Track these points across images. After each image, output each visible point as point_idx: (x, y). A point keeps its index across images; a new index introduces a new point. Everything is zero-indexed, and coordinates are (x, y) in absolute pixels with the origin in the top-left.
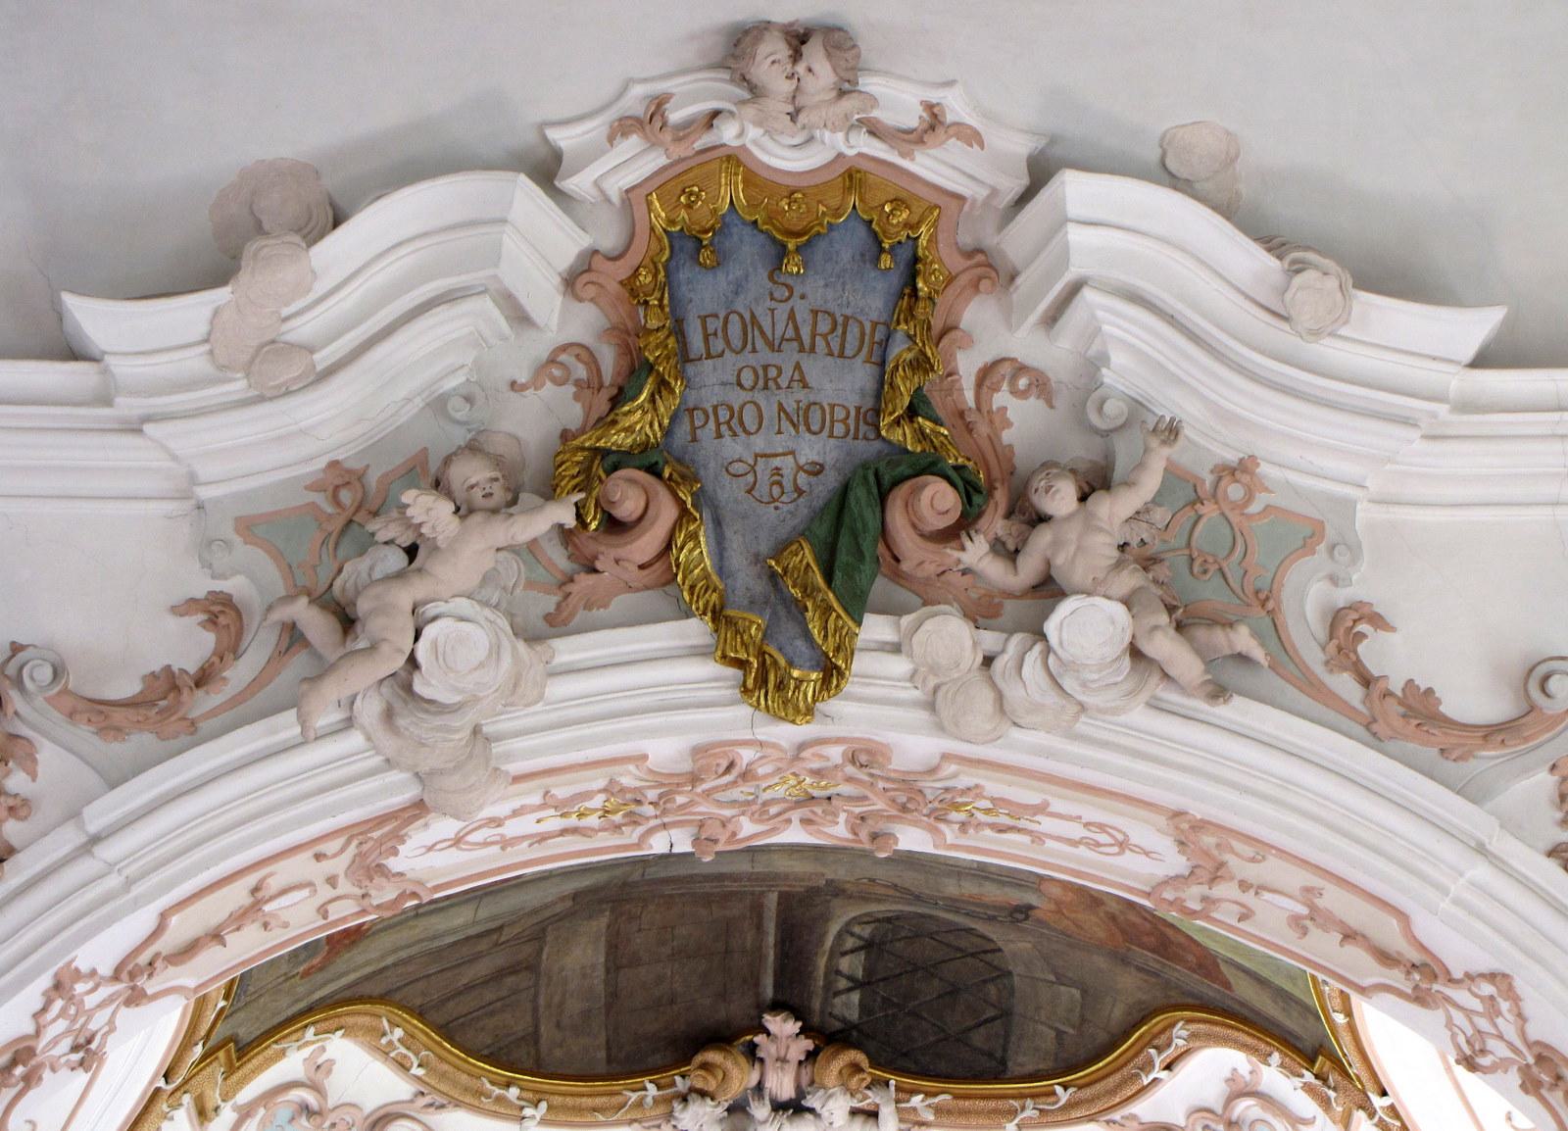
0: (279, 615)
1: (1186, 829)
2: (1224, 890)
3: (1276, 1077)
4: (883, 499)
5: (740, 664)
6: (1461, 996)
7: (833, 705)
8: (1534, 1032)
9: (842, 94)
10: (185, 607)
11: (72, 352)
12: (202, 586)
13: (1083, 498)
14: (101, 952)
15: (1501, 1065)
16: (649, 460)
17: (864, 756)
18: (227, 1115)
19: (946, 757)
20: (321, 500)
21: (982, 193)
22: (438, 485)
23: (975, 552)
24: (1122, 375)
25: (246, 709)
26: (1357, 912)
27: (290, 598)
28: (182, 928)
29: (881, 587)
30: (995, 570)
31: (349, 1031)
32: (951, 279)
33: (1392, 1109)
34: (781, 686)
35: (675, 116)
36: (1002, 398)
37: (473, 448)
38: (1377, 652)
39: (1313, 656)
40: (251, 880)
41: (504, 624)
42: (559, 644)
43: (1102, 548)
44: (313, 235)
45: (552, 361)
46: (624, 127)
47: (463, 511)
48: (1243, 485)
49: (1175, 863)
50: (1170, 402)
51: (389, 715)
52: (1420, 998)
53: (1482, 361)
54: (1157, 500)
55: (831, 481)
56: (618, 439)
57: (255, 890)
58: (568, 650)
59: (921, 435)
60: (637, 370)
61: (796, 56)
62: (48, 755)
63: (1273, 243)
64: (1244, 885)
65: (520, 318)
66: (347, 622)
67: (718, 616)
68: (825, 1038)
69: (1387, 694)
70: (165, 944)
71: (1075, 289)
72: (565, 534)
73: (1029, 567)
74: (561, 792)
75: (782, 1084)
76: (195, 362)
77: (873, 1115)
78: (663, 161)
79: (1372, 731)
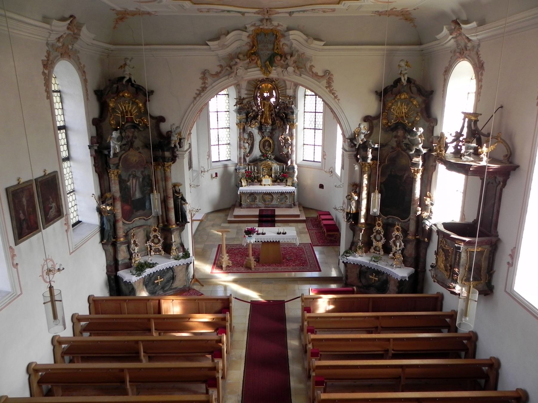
4: (274, 57)
10: (218, 66)
11: (208, 45)
12: (219, 64)
16: (254, 53)
23: (282, 61)
27: (227, 66)
29: (274, 64)
30: (283, 63)
32: (280, 37)
39: (308, 70)
42: (248, 70)
43: (292, 62)
45: (247, 44)
50: (298, 48)
51: (235, 76)
53: (323, 45)
55: (270, 55)
58: (249, 70)
60: (254, 46)
61: (267, 22)
63: (307, 35)
73: (286, 63)
76: (217, 46)
79: (312, 77)
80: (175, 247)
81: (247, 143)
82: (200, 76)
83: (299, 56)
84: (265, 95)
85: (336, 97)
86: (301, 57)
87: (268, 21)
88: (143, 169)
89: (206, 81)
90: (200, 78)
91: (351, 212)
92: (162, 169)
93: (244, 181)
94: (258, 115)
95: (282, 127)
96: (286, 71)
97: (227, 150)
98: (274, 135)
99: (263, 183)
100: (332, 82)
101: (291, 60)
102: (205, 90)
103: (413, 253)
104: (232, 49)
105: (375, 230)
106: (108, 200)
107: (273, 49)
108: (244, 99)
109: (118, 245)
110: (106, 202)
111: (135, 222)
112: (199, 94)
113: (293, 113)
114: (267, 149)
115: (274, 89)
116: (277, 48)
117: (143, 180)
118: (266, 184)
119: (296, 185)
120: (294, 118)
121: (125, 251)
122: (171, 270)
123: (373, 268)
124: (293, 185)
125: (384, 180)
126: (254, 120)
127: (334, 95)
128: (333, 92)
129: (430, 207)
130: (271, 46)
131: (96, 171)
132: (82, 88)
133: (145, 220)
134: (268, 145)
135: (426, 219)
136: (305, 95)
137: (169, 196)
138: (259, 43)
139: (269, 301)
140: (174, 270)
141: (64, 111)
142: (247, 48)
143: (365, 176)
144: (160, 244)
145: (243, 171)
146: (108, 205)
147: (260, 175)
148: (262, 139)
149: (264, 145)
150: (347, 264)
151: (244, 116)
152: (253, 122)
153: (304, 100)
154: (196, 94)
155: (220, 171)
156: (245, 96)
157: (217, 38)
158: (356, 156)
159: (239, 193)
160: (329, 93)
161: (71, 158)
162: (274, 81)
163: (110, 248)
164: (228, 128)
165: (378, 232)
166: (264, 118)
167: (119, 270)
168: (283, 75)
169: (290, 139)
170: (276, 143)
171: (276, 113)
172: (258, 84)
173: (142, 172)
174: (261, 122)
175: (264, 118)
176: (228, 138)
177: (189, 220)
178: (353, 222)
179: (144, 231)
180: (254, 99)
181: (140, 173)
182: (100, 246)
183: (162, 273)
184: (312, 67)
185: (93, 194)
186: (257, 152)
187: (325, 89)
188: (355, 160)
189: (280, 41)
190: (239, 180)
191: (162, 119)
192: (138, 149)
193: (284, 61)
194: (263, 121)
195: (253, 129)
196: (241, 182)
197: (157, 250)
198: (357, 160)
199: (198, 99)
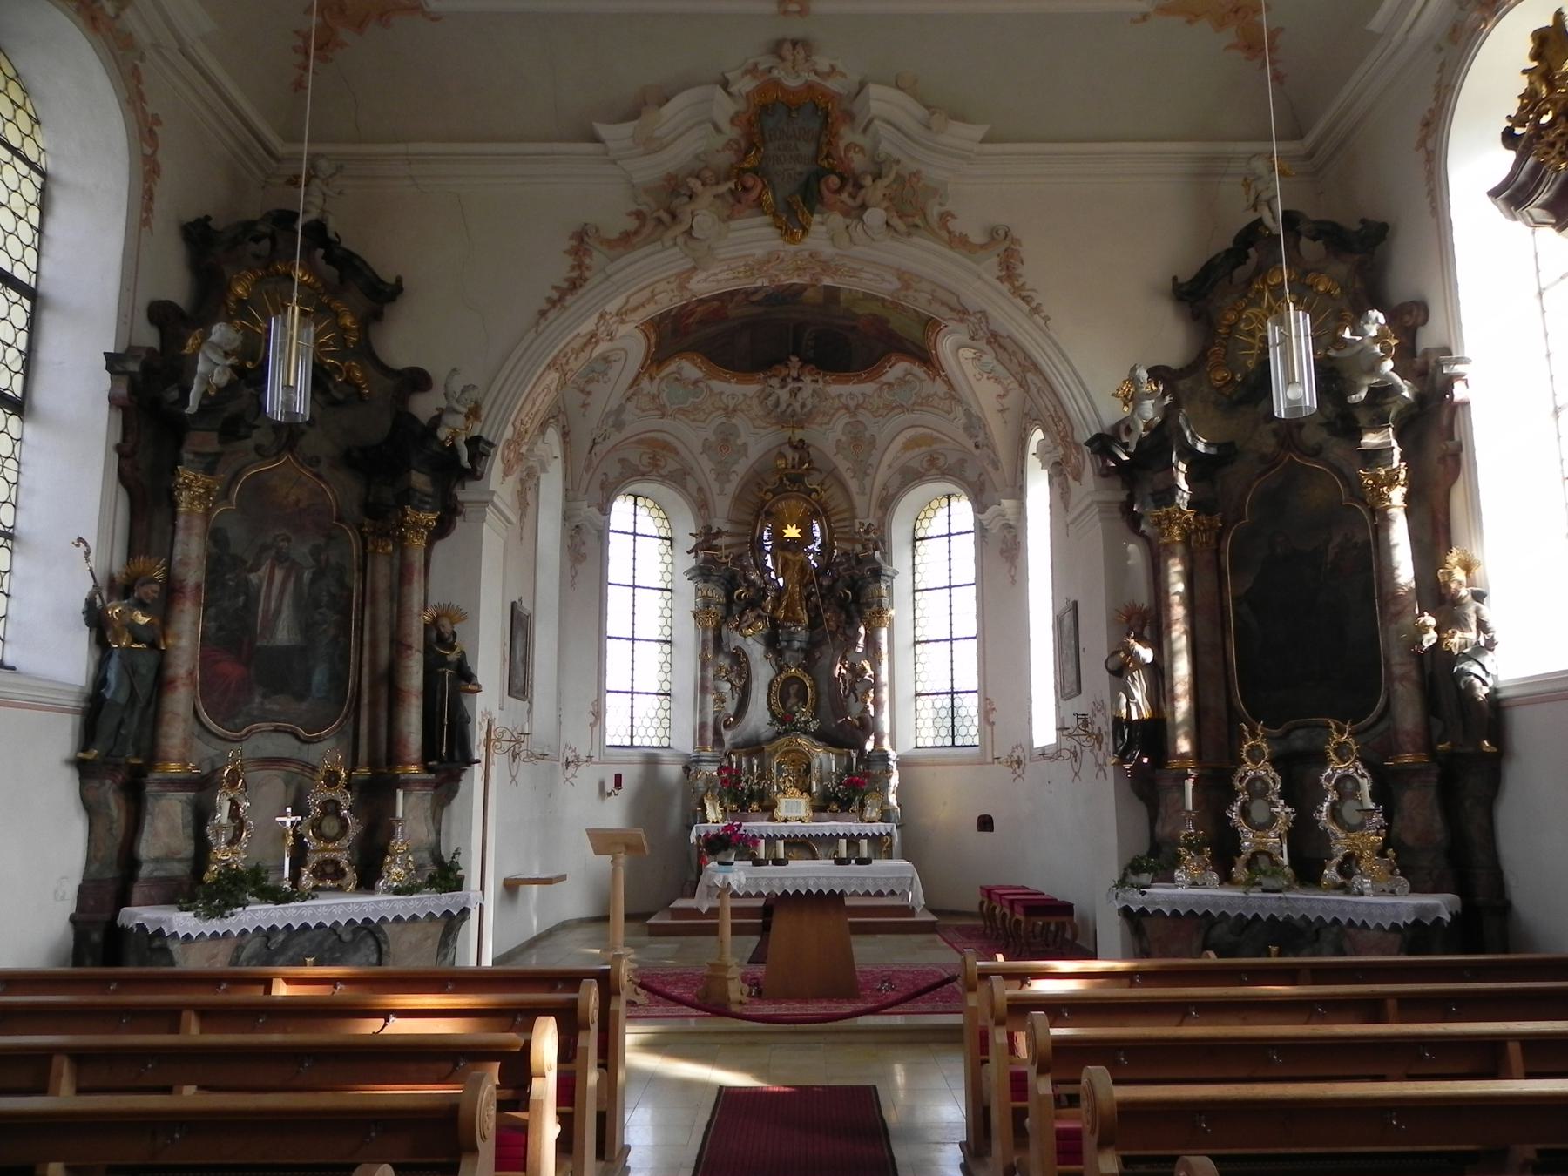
0: (655, 215)
1: (901, 274)
2: (911, 292)
3: (918, 370)
4: (818, 181)
5: (780, 228)
6: (972, 319)
7: (806, 239)
8: (991, 327)
9: (807, 61)
10: (630, 214)
11: (596, 139)
12: (634, 207)
13: (874, 181)
14: (613, 306)
15: (982, 338)
16: (755, 171)
18: (657, 380)
19: (837, 254)
20: (666, 183)
21: (846, 92)
22: (697, 177)
23: (845, 196)
24: (885, 148)
27: (658, 210)
28: (634, 302)
29: (818, 207)
30: (849, 201)
31: (687, 359)
33: (946, 375)
34: (791, 234)
35: (761, 67)
36: (851, 154)
37: (706, 167)
38: (953, 225)
40: (651, 289)
41: (716, 217)
43: (879, 194)
44: (661, 105)
45: (728, 144)
47: (704, 184)
49: (897, 284)
51: (686, 243)
53: (984, 141)
54: (894, 181)
56: (746, 165)
57: (652, 292)
58: (734, 224)
59: (829, 163)
60: (752, 145)
61: (794, 48)
62: (595, 254)
63: (928, 107)
64: (916, 291)
65: (718, 130)
66: (674, 216)
67: (774, 215)
68: (805, 362)
69: (955, 236)
71: (870, 122)
72: (732, 192)
73: (859, 200)
74: (733, 266)
75: (794, 373)
77: (817, 381)
78: (758, 83)
80: (403, 843)
81: (728, 680)
82: (568, 244)
84: (792, 532)
85: (1036, 310)
86: (908, 185)
87: (800, 48)
88: (321, 541)
89: (587, 261)
90: (565, 252)
91: (1135, 716)
92: (397, 555)
93: (715, 809)
94: (765, 597)
95: (844, 634)
96: (859, 227)
97: (661, 714)
99: (781, 812)
100: (1018, 263)
101: (875, 192)
102: (581, 286)
103: (1438, 823)
104: (677, 156)
105: (1241, 780)
106: (143, 585)
107: (816, 158)
108: (719, 533)
109: (150, 789)
110: (136, 595)
111: (253, 738)
112: (561, 299)
113: (877, 574)
114: (793, 706)
115: (815, 515)
116: (828, 156)
117: (313, 581)
118: (789, 815)
120: (884, 592)
121: (179, 821)
122: (371, 942)
123: (1264, 917)
124: (885, 819)
125: (1248, 586)
126: (752, 610)
127: (1028, 303)
128: (1024, 294)
129: (1471, 611)
130: (807, 149)
131: (123, 477)
132: (131, 164)
133: (297, 737)
134: (796, 695)
135: (1468, 657)
136: (915, 540)
138: (767, 136)
139: (803, 1090)
140: (386, 942)
141: (45, 244)
142: (726, 159)
143: (1175, 569)
144: (345, 843)
145: (712, 769)
146: (142, 605)
147: (771, 786)
148: (777, 675)
149: (784, 693)
150: (1145, 922)
151: (718, 595)
152: (750, 616)
153: (910, 554)
155: (631, 775)
156: (726, 527)
157: (633, 114)
158: (1126, 508)
159: (693, 839)
160: (1011, 296)
161: (31, 408)
162: (817, 492)
163: (116, 808)
164: (666, 642)
165: (1257, 789)
166: (784, 603)
167: (133, 902)
168: (851, 240)
169: (868, 668)
170: (824, 687)
171: (823, 592)
172: (767, 501)
173: (316, 552)
175: (784, 603)
176: (666, 673)
177: (478, 752)
178: (1145, 760)
179: (287, 784)
180: (752, 550)
181: (305, 549)
182: (66, 785)
183: (327, 945)
184: (945, 217)
185: (80, 540)
186: (759, 717)
187: (997, 283)
188: (1121, 526)
190: (697, 801)
191: (418, 380)
192: (314, 461)
193: (853, 196)
194: (781, 613)
195: (749, 640)
196: (704, 809)
197: (329, 869)
198: (1134, 522)
199: (552, 315)
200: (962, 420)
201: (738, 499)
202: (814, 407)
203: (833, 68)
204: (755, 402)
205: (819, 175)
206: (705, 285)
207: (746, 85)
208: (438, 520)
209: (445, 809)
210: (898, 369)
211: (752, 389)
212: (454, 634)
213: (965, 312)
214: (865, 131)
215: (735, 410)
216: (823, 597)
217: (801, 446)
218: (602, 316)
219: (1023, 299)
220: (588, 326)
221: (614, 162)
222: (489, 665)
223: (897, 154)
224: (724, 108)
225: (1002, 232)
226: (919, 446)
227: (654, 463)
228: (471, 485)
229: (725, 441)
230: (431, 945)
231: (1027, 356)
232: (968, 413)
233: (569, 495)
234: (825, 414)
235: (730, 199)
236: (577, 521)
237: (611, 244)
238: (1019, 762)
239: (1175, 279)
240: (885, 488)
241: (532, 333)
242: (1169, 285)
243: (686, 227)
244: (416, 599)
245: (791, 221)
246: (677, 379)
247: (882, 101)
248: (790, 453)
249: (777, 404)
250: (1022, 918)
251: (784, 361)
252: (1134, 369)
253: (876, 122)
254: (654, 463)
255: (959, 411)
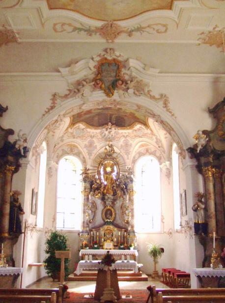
3: (143, 127)
11: (59, 71)
12: (68, 88)
14: (62, 113)
17: (115, 101)
22: (85, 81)
23: (123, 86)
24: (134, 74)
25: (72, 97)
26: (150, 111)
28: (68, 112)
29: (116, 88)
30: (125, 87)
36: (125, 75)
46: (97, 56)
48: (141, 154)
52: (154, 117)
53: (159, 73)
56: (97, 78)
58: (94, 93)
60: (99, 73)
62: (58, 100)
65: (90, 69)
66: (79, 90)
67: (105, 90)
70: (67, 113)
75: (110, 127)
83: (138, 82)
85: (173, 115)
94: (101, 187)
95: (123, 197)
98: (115, 204)
99: (105, 247)
101: (131, 85)
107: (116, 76)
108: (89, 170)
112: (49, 111)
119: (137, 258)
130: (113, 74)
134: (109, 214)
137: (7, 200)
142: (92, 76)
150: (203, 280)
151: (88, 185)
152: (97, 192)
154: (45, 111)
156: (91, 168)
157: (69, 65)
174: (103, 193)
184: (149, 91)
186: (99, 220)
188: (195, 171)
189: (121, 71)
191: (11, 132)
193: (125, 86)
194: (105, 191)
199: (46, 115)
200: (155, 140)
201: (95, 161)
202: (115, 136)
203: (120, 55)
204: (99, 135)
205: (116, 81)
206: (85, 108)
207: (98, 59)
208: (15, 169)
209: (14, 246)
210: (138, 126)
211: (98, 131)
212: (18, 199)
213: (155, 115)
214: (128, 69)
215: (94, 136)
216: (117, 187)
217: (111, 146)
218: (59, 116)
219: (170, 112)
220: (55, 118)
221: (63, 77)
222: (27, 207)
223: (136, 76)
224: (92, 64)
225: (164, 96)
226: (143, 146)
227: (71, 150)
228: (24, 159)
229: (91, 145)
230: (10, 282)
231: (171, 127)
232: (156, 138)
233: (49, 159)
234: (118, 138)
235: (93, 86)
236: (50, 166)
237: (62, 97)
238: (171, 233)
239: (209, 108)
240: (134, 158)
241: (41, 120)
242: (208, 110)
243: (81, 93)
244: (9, 189)
245: (109, 91)
246: (78, 129)
247: (132, 63)
248: (107, 147)
249: (105, 135)
250: (176, 278)
251: (107, 124)
252: (198, 131)
253: (131, 68)
254: (71, 150)
255: (154, 137)
